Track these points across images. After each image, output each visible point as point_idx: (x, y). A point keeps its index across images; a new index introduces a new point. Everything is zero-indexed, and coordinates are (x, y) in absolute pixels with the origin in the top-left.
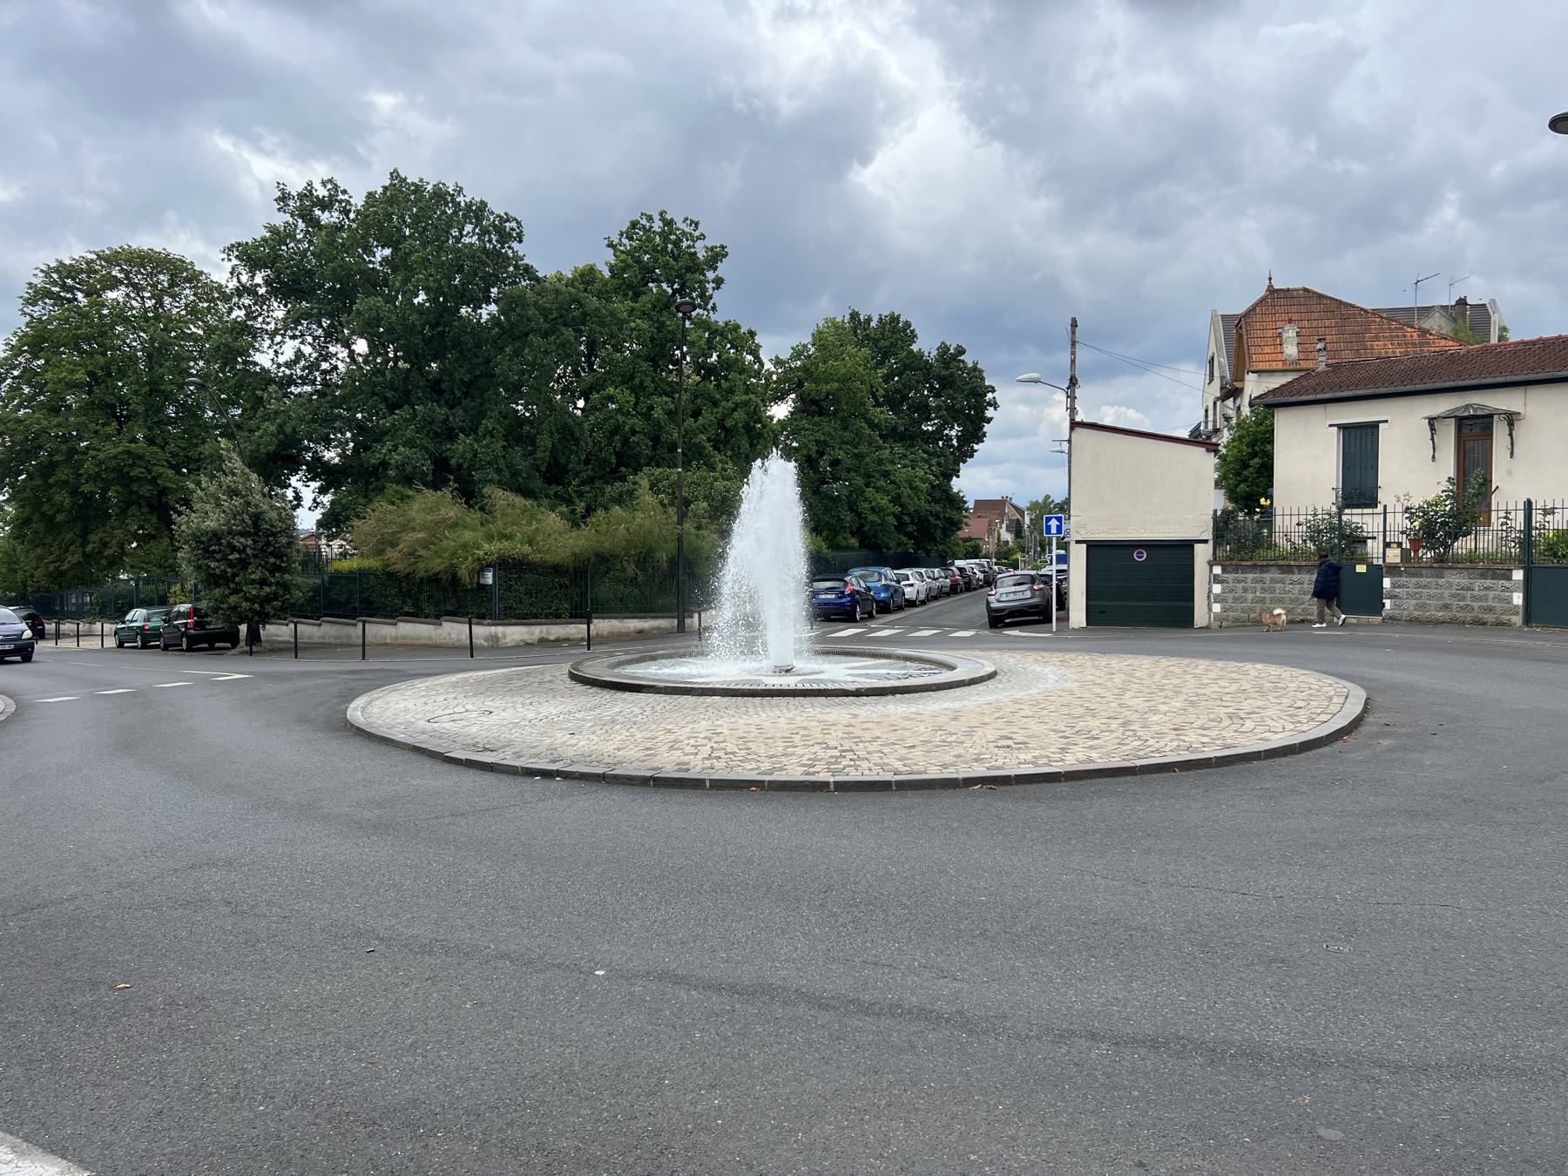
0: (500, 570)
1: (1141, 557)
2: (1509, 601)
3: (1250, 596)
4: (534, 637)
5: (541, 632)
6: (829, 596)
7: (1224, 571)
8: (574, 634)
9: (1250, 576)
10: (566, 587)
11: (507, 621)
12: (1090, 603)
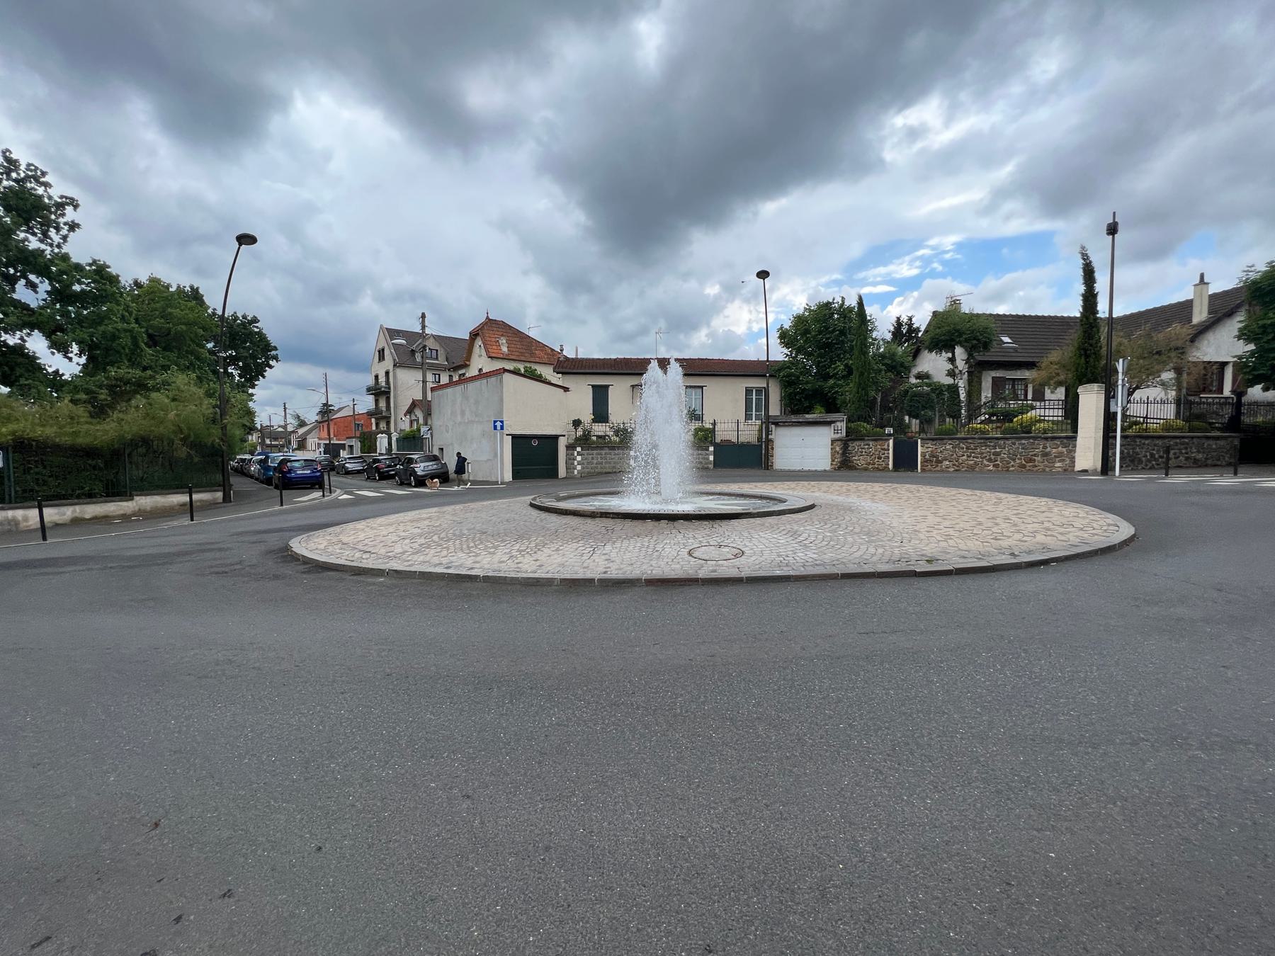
0: (13, 452)
1: (535, 443)
2: (708, 459)
3: (595, 461)
4: (65, 517)
5: (74, 511)
6: (305, 472)
7: (582, 450)
8: (114, 511)
9: (595, 452)
10: (100, 469)
11: (26, 504)
12: (514, 468)
